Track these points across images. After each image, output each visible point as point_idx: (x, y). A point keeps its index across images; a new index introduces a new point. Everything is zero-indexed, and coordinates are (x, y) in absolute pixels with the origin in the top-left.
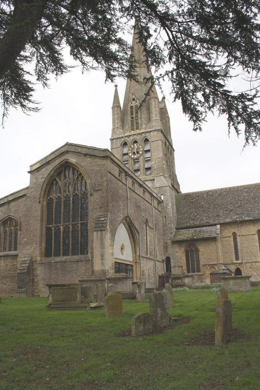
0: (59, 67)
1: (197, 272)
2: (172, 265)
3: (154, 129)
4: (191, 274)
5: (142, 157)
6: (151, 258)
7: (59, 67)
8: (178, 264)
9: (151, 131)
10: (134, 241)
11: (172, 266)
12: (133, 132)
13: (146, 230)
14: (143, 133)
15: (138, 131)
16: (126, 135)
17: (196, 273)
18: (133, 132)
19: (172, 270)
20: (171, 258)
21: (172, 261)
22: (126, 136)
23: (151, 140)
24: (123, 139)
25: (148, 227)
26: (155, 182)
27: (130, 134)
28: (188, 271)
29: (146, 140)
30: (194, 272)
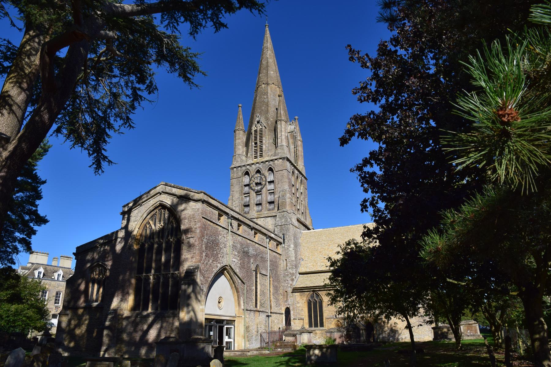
0: (34, 232)
1: (315, 327)
2: (292, 317)
3: (279, 157)
4: (313, 328)
5: (264, 189)
6: (261, 310)
7: (34, 232)
8: (299, 316)
9: (276, 159)
10: (238, 292)
11: (292, 319)
12: (255, 160)
13: (256, 278)
14: (266, 161)
15: (259, 160)
16: (248, 163)
17: (319, 328)
18: (255, 160)
19: (292, 323)
20: (291, 309)
21: (292, 312)
22: (248, 165)
23: (276, 169)
24: (244, 168)
25: (258, 275)
26: (278, 219)
27: (253, 162)
28: (310, 326)
29: (271, 169)
30: (316, 326)
